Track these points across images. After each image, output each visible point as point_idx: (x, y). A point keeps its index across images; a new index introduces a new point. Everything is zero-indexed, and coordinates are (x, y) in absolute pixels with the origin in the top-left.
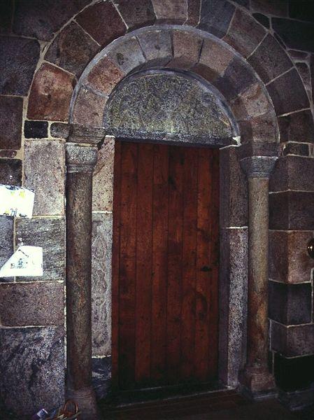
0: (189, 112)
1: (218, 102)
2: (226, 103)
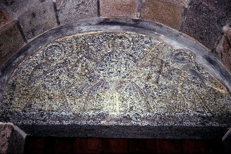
0: (149, 78)
1: (201, 61)
2: (212, 57)
